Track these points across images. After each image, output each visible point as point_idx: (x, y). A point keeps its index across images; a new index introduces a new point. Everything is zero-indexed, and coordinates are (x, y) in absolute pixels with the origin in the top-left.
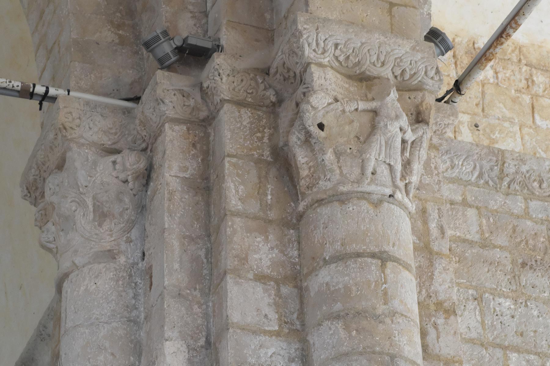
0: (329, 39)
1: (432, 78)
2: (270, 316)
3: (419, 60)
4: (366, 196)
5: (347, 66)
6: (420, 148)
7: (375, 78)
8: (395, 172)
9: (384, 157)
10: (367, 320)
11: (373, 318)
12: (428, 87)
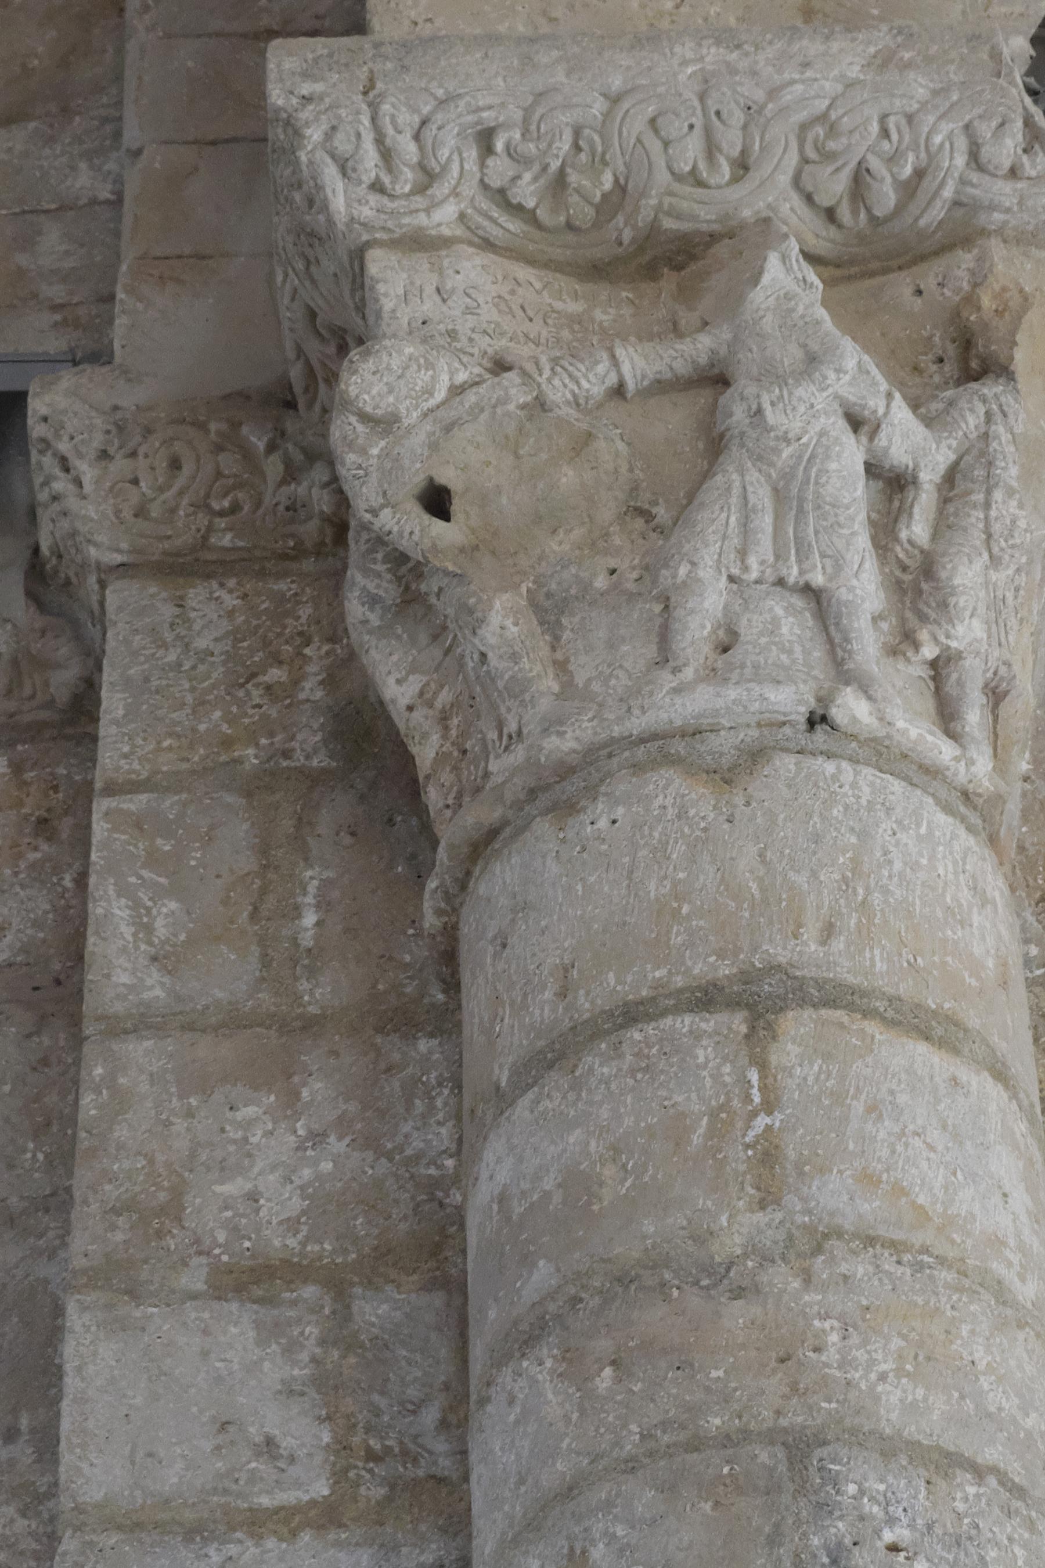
0: (439, 118)
1: (1013, 173)
2: (287, 1443)
3: (924, 105)
4: (678, 747)
5: (570, 226)
6: (989, 492)
7: (713, 238)
8: (839, 616)
9: (771, 559)
10: (667, 1298)
11: (696, 1283)
12: (998, 216)
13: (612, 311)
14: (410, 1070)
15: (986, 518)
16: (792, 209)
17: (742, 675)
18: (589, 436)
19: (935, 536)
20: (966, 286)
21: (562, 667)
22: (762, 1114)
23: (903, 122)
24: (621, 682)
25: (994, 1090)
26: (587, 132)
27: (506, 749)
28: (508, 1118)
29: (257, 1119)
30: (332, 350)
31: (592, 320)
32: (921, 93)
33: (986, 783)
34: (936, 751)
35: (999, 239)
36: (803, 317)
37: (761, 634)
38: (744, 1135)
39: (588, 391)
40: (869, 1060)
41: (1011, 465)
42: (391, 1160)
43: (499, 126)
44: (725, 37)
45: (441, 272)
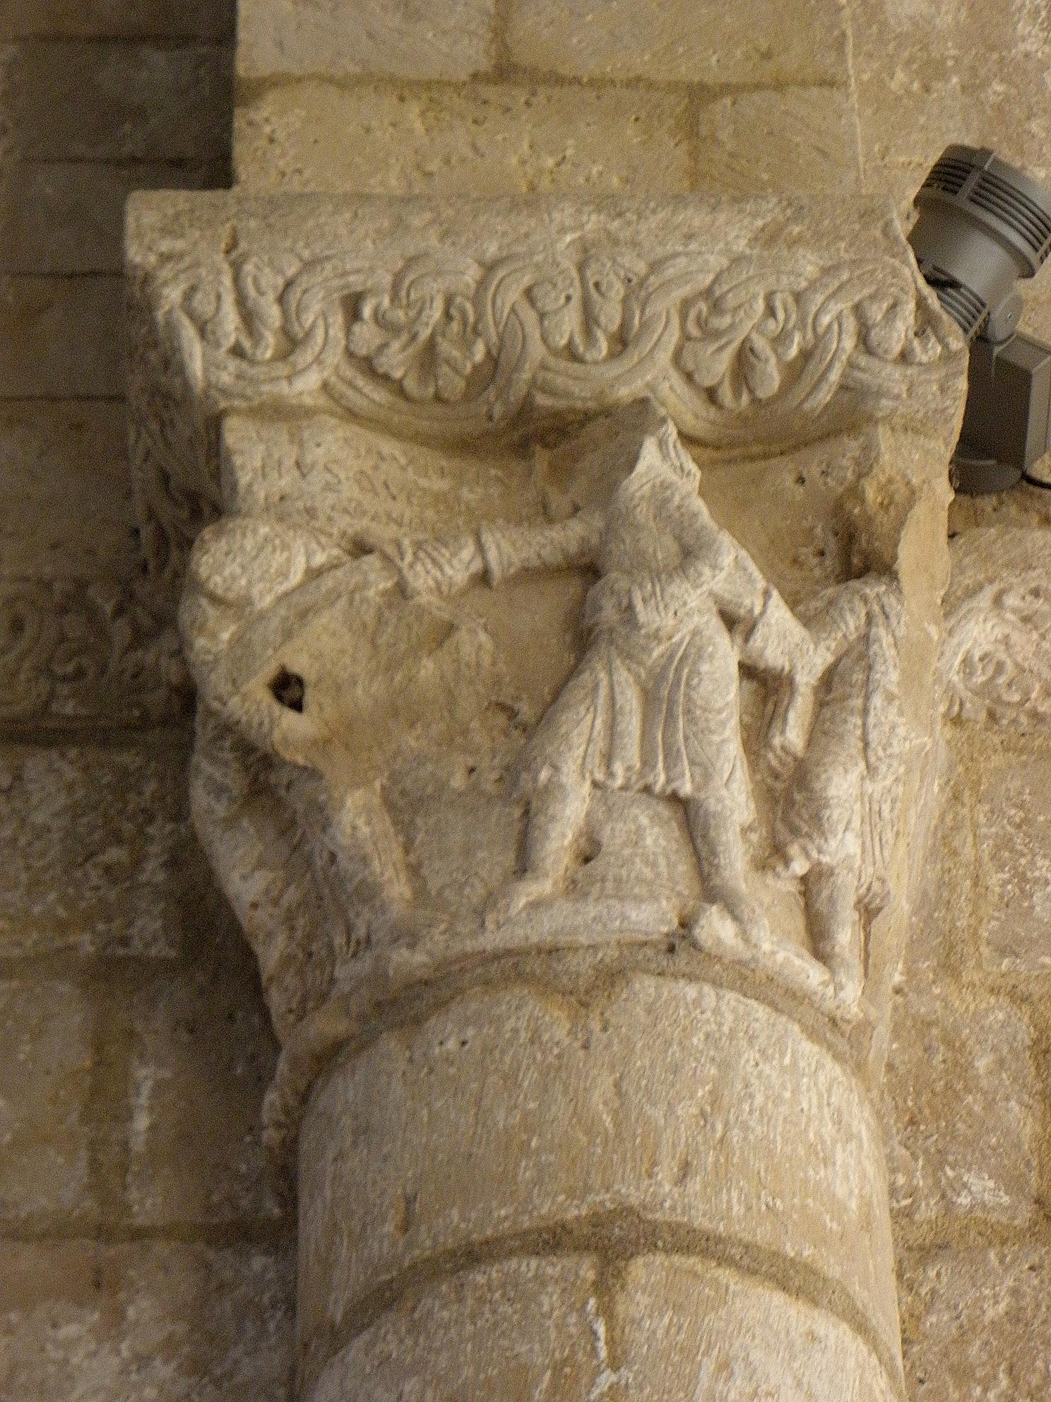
0: (304, 281)
1: (905, 357)
3: (813, 285)
5: (438, 398)
6: (867, 698)
7: (588, 417)
8: (706, 827)
13: (480, 490)
14: (243, 1289)
15: (864, 725)
16: (671, 388)
17: (602, 889)
18: (450, 628)
19: (810, 743)
20: (850, 475)
21: (415, 871)
22: (608, 1371)
23: (790, 300)
24: (476, 892)
25: (856, 1346)
26: (458, 300)
27: (354, 955)
28: (342, 1360)
29: (79, 1338)
30: (185, 514)
31: (458, 499)
32: (810, 270)
33: (855, 1009)
34: (803, 976)
35: (888, 427)
36: (679, 507)
37: (624, 845)
38: (588, 1393)
39: (451, 578)
40: (723, 1312)
41: (891, 669)
42: (219, 1387)
43: (370, 291)
44: (606, 202)
45: (301, 444)
